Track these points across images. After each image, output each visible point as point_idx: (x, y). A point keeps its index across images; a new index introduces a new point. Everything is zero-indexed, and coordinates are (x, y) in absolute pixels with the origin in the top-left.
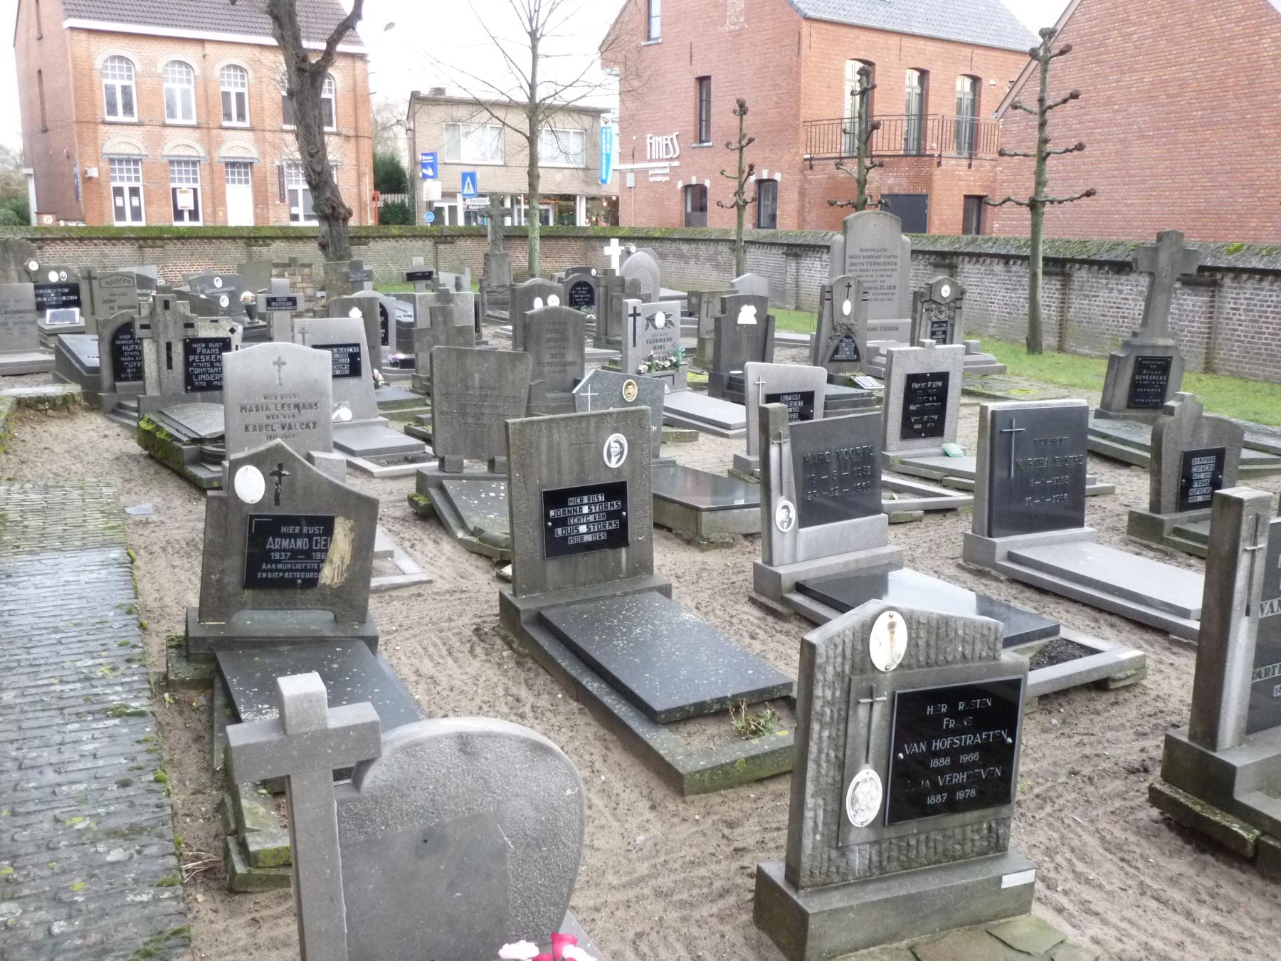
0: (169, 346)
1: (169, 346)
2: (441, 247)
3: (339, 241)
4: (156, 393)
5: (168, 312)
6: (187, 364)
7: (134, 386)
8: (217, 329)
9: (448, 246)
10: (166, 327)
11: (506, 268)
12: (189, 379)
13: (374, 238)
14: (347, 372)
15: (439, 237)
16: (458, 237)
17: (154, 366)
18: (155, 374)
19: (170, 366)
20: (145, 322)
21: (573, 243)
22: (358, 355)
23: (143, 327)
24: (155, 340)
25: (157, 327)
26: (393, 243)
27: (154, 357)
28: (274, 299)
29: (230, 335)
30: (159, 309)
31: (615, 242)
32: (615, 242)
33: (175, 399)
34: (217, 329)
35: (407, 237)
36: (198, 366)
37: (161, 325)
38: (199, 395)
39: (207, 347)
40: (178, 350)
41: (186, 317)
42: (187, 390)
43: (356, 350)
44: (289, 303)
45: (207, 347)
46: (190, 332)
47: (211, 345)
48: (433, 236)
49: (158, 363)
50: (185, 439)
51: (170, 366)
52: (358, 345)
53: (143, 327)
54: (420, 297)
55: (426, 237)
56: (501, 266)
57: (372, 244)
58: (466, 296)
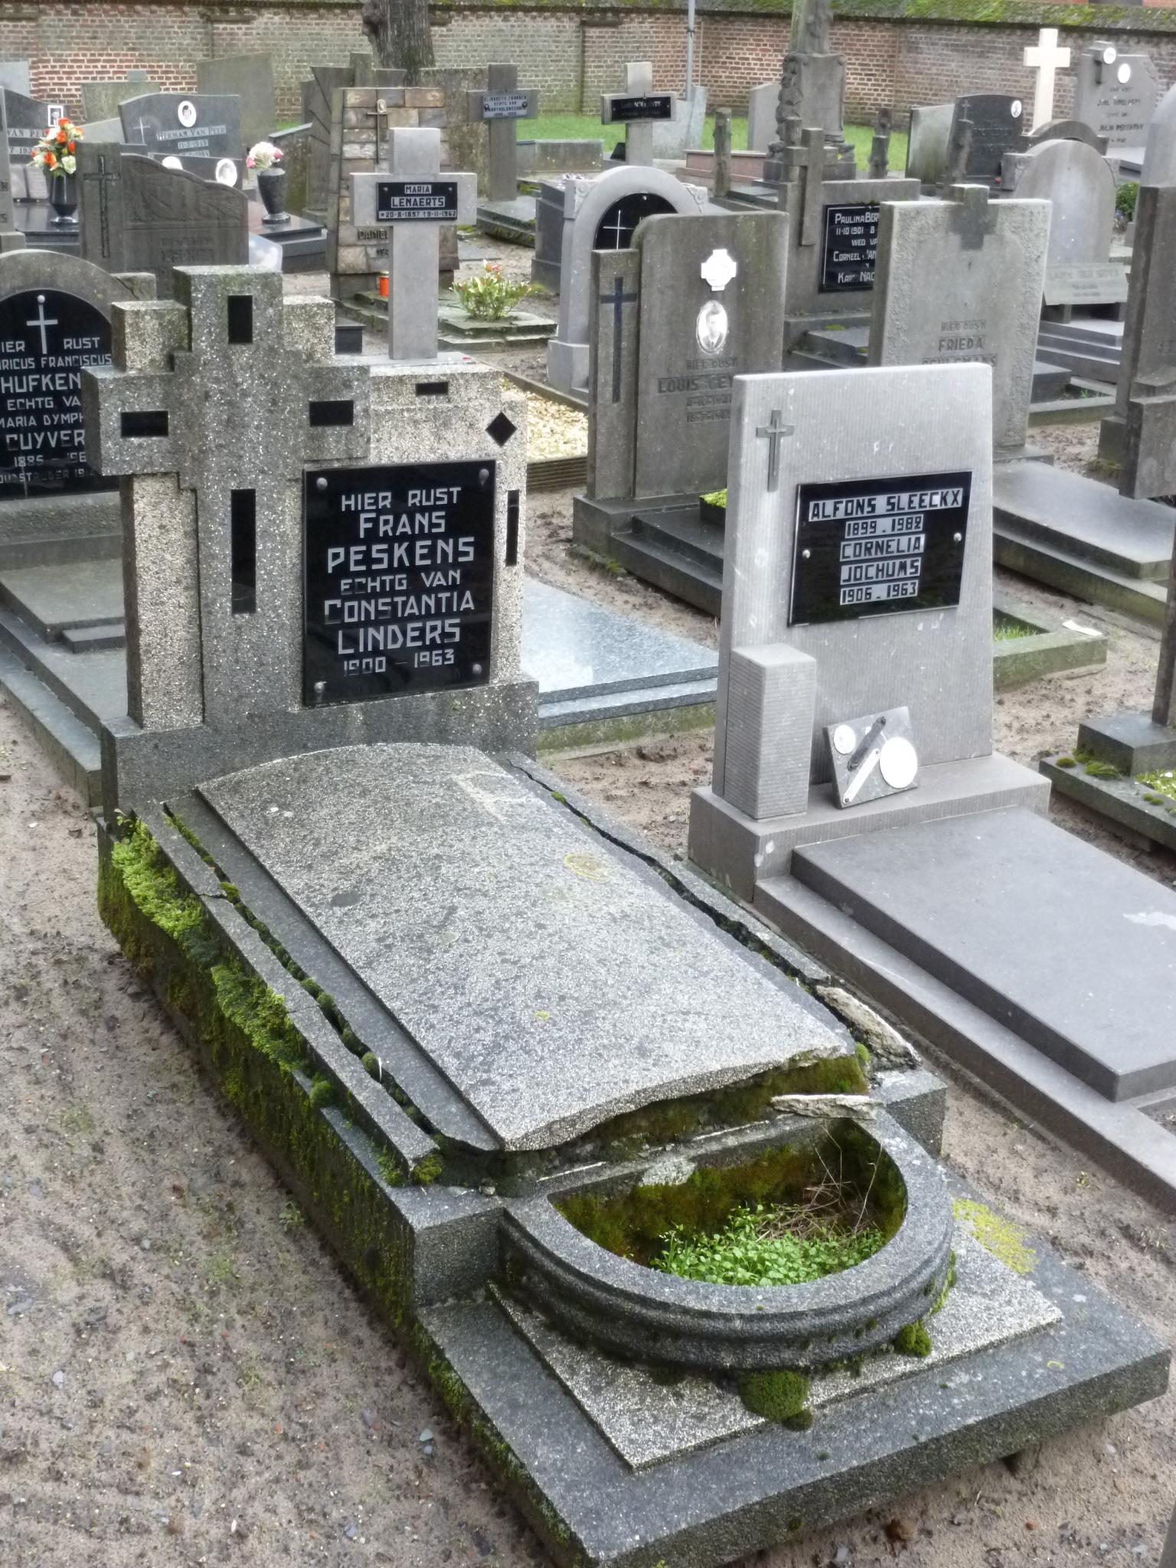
0: (243, 505)
1: (243, 505)
2: (593, 32)
3: (409, 15)
4: (183, 717)
5: (243, 354)
6: (318, 582)
7: (38, 517)
8: (442, 422)
9: (608, 31)
10: (233, 423)
11: (833, 94)
12: (319, 637)
13: (460, 10)
14: (912, 589)
15: (591, 11)
16: (628, 11)
17: (178, 598)
18: (180, 634)
19: (244, 598)
20: (144, 403)
21: (867, 32)
22: (958, 518)
23: (136, 425)
24: (183, 481)
25: (193, 422)
26: (497, 21)
27: (177, 559)
28: (397, 189)
29: (490, 448)
30: (208, 339)
31: (1049, 36)
32: (1049, 36)
33: (268, 734)
34: (442, 422)
35: (527, 10)
36: (359, 593)
37: (212, 414)
38: (356, 711)
39: (399, 507)
40: (281, 524)
41: (324, 375)
42: (308, 698)
43: (951, 498)
44: (439, 201)
45: (399, 507)
46: (335, 447)
47: (416, 497)
48: (578, 10)
49: (197, 584)
50: (412, 1144)
51: (244, 598)
52: (961, 480)
53: (136, 425)
54: (905, 214)
55: (565, 10)
56: (822, 89)
57: (457, 24)
58: (1030, 213)
